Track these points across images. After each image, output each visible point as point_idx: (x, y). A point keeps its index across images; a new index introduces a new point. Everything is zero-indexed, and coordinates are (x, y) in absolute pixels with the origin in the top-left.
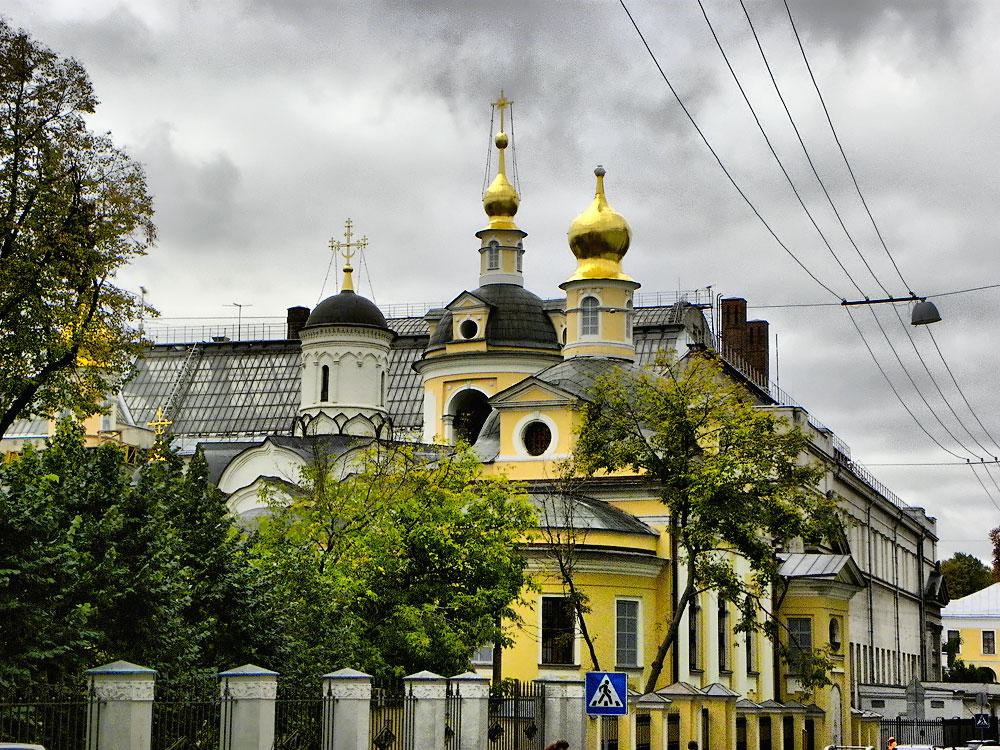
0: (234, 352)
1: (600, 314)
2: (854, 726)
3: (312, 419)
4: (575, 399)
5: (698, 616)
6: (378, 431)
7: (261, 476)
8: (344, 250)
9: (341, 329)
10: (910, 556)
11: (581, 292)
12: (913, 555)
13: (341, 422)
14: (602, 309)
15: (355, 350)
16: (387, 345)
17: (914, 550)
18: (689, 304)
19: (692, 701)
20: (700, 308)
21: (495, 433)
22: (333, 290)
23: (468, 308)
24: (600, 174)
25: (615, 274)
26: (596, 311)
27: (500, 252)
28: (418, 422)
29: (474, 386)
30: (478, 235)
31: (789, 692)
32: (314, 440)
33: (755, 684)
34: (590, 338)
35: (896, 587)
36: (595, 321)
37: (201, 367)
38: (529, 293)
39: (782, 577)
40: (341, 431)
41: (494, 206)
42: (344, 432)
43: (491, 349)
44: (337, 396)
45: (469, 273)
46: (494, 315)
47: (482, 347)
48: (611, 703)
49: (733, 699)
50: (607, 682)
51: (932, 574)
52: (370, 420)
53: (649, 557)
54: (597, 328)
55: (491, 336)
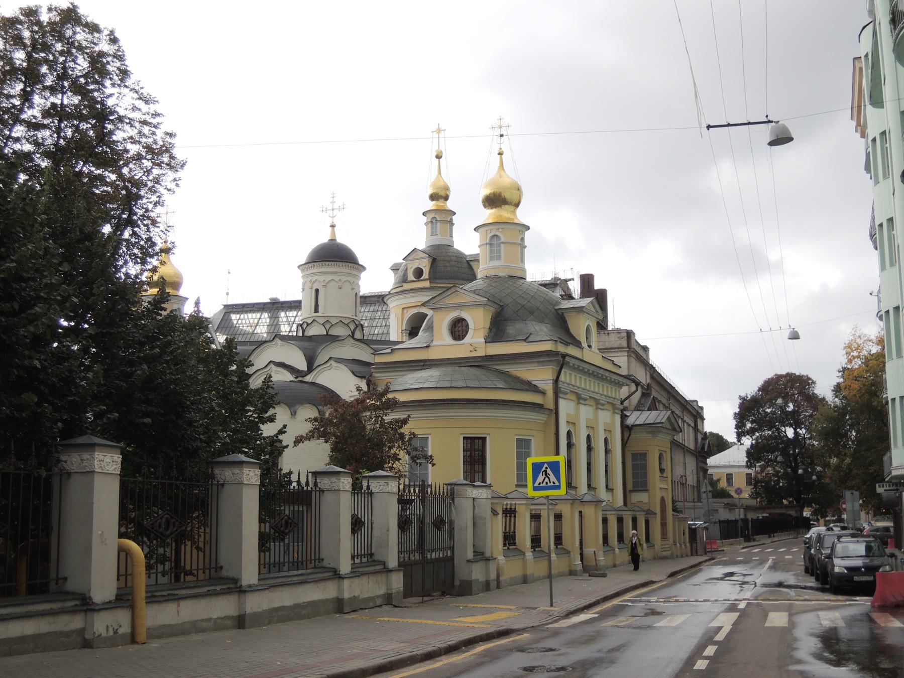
0: (282, 307)
1: (502, 245)
2: (674, 523)
3: (308, 325)
5: (573, 450)
6: (353, 333)
7: (271, 362)
8: (330, 213)
9: (327, 263)
10: (691, 428)
11: (489, 231)
12: (692, 427)
13: (328, 326)
14: (503, 243)
15: (337, 278)
17: (693, 425)
18: (560, 279)
19: (571, 504)
20: (566, 281)
22: (324, 239)
23: (417, 259)
24: (500, 154)
25: (513, 219)
26: (499, 245)
27: (438, 224)
30: (424, 214)
31: (633, 502)
32: (304, 338)
33: (611, 496)
35: (684, 445)
36: (499, 251)
37: (263, 317)
38: (457, 250)
39: (628, 426)
40: (327, 333)
42: (329, 333)
45: (420, 239)
46: (434, 261)
47: (427, 284)
48: (550, 482)
49: (600, 503)
50: (546, 468)
51: (702, 439)
52: (347, 325)
53: (538, 407)
54: (500, 256)
55: (433, 277)
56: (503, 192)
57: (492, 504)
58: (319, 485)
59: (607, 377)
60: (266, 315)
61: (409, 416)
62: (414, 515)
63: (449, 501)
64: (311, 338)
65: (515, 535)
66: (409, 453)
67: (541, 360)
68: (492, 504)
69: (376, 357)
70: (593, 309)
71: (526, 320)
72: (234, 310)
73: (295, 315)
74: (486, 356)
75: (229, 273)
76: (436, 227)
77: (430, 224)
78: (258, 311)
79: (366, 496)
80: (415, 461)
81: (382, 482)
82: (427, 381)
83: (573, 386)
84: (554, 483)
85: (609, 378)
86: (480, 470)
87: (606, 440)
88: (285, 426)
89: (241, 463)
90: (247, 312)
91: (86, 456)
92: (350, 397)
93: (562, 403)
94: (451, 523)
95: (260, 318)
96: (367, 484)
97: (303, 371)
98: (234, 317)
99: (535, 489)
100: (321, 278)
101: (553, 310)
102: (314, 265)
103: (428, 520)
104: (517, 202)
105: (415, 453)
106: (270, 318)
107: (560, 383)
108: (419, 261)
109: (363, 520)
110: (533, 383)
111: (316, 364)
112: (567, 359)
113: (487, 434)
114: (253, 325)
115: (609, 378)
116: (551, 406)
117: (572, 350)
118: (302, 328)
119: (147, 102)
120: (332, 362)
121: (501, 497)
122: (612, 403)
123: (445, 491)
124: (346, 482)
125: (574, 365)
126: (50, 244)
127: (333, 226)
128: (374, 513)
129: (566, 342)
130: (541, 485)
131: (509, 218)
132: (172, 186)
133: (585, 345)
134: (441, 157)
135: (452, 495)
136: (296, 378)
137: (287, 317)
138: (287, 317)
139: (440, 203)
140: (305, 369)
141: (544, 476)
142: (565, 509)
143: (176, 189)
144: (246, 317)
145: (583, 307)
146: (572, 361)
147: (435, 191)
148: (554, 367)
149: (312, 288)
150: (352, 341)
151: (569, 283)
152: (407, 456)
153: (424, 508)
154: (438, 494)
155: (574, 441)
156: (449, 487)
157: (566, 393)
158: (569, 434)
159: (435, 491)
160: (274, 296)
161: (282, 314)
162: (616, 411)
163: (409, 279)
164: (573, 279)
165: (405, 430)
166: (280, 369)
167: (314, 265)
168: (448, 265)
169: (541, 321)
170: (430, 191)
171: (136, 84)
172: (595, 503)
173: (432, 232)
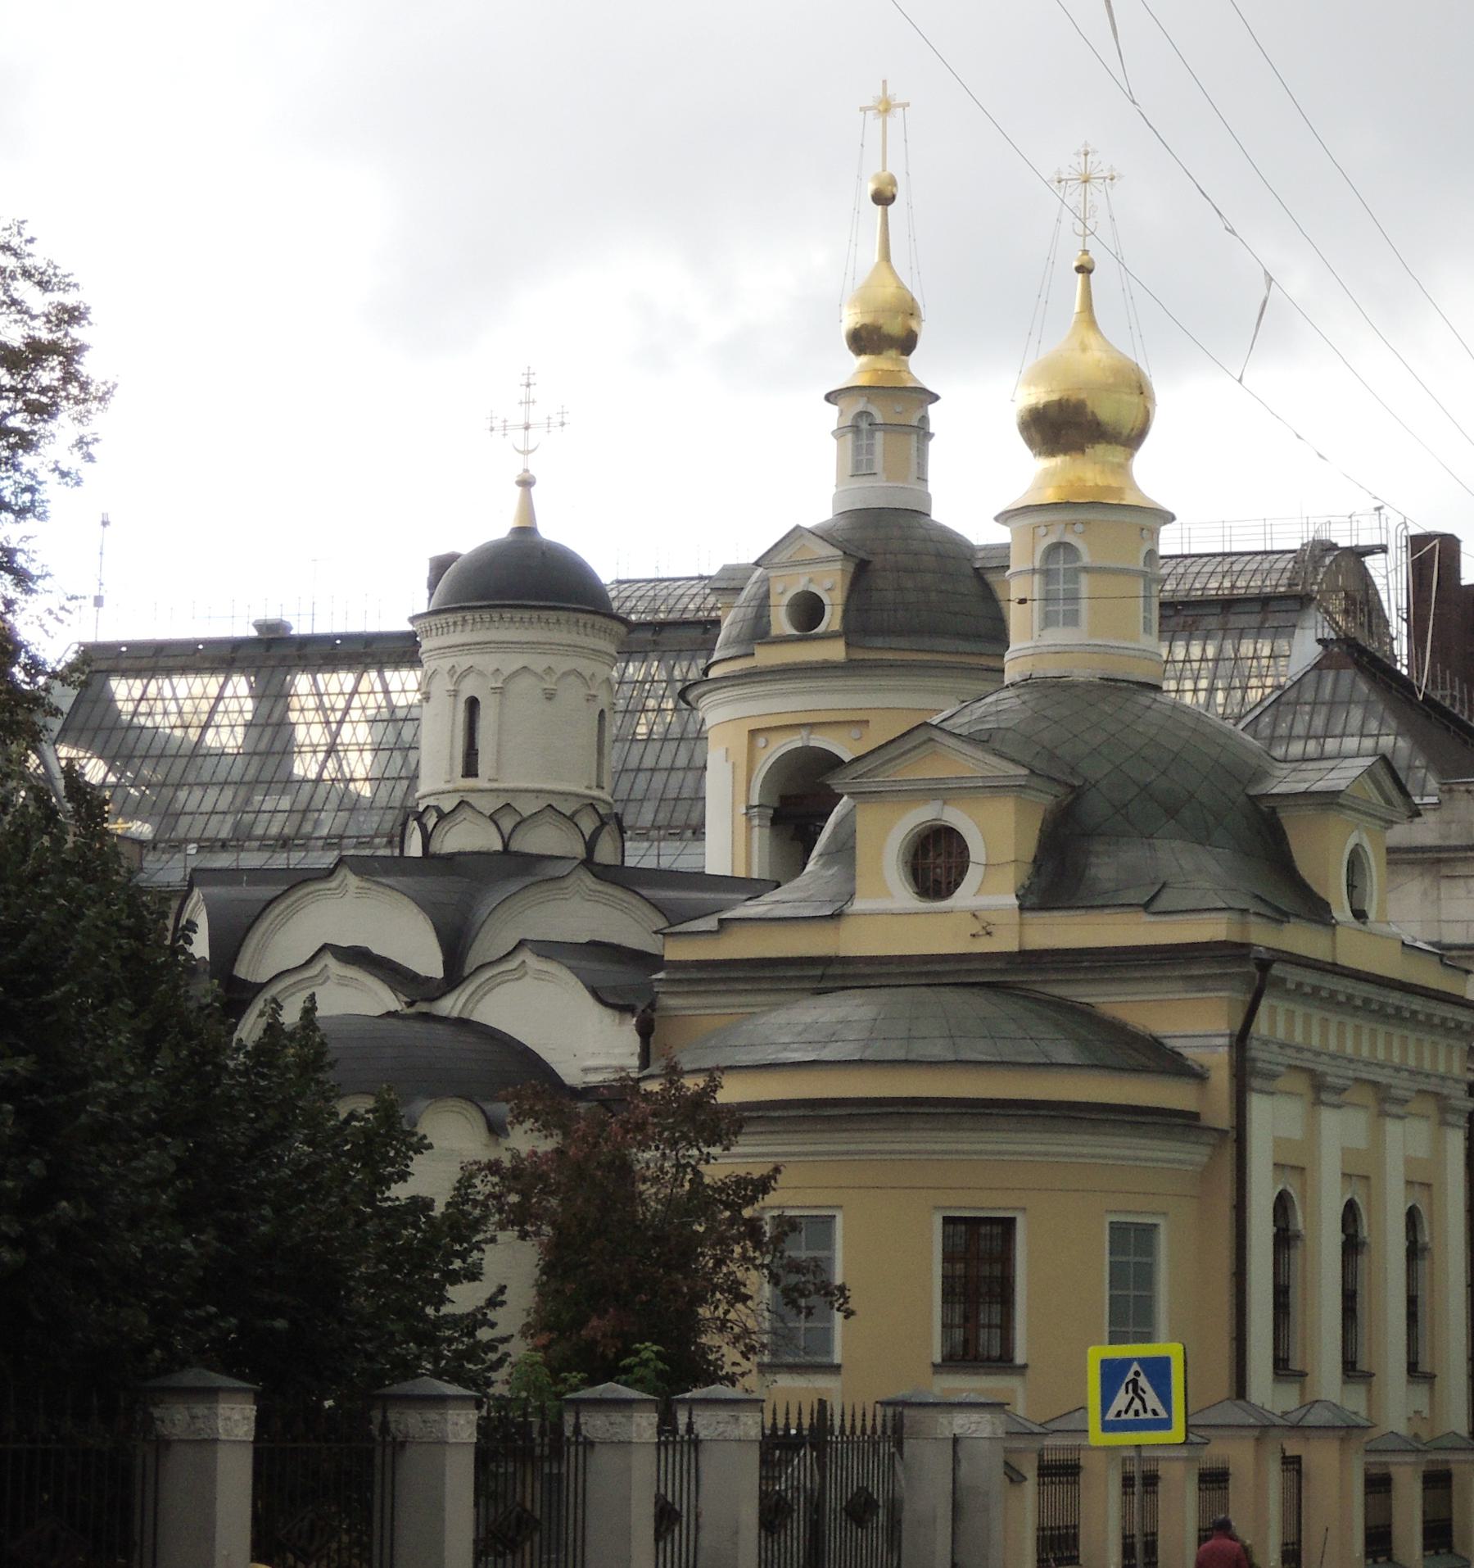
0: (299, 657)
1: (1084, 580)
3: (442, 816)
4: (1025, 772)
6: (590, 846)
7: (325, 948)
11: (1042, 530)
13: (507, 824)
14: (1086, 569)
15: (538, 663)
16: (612, 650)
18: (1334, 547)
19: (1257, 1439)
20: (1358, 554)
21: (844, 851)
22: (497, 527)
24: (1084, 269)
25: (1119, 491)
26: (1074, 574)
27: (879, 436)
28: (694, 821)
29: (820, 741)
30: (830, 397)
32: (433, 862)
33: (1426, 1400)
34: (1059, 636)
37: (228, 692)
40: (506, 845)
41: (864, 334)
42: (515, 846)
43: (859, 655)
44: (499, 766)
46: (861, 574)
47: (836, 651)
50: (1137, 1373)
52: (571, 818)
53: (1182, 1123)
55: (856, 629)
56: (1089, 403)
57: (1007, 1451)
58: (584, 1432)
59: (1414, 1013)
60: (240, 685)
61: (777, 1170)
62: (798, 1488)
63: (885, 1448)
64: (452, 863)
65: (1076, 1537)
66: (774, 1279)
67: (1196, 972)
68: (1007, 1451)
69: (670, 942)
70: (1376, 797)
71: (1151, 836)
72: (125, 664)
73: (348, 688)
74: (1022, 953)
75: (105, 524)
76: (870, 449)
77: (850, 436)
78: (213, 671)
79: (685, 1449)
80: (793, 1303)
81: (723, 1414)
82: (831, 1039)
83: (1299, 1049)
84: (1154, 1412)
85: (1421, 1017)
86: (997, 1320)
87: (1412, 1217)
88: (502, 1290)
89: (441, 1400)
90: (169, 672)
91: (200, 1410)
92: (586, 1070)
93: (1259, 1107)
94: (895, 1509)
95: (219, 698)
96: (687, 1420)
97: (429, 979)
98: (123, 690)
99: (1107, 1427)
100: (486, 662)
101: (1242, 798)
102: (464, 620)
103: (834, 1500)
104: (1138, 424)
105: (793, 1279)
106: (257, 695)
107: (1255, 1043)
108: (808, 569)
109: (677, 1507)
110: (1169, 1043)
111: (473, 960)
112: (1277, 970)
113: (1015, 1209)
114: (195, 722)
115: (1421, 1017)
116: (1220, 1114)
117: (1300, 939)
118: (423, 827)
119: (44, 285)
120: (526, 956)
121: (1032, 1433)
122: (1436, 1095)
123: (879, 1420)
124: (644, 1423)
125: (1299, 985)
126: (127, 1005)
127: (526, 483)
128: (702, 1490)
129: (1277, 909)
130: (1124, 1416)
131: (1108, 489)
132: (72, 461)
133: (1342, 911)
134: (893, 198)
135: (897, 1433)
136: (410, 1004)
137: (319, 695)
138: (319, 695)
139: (884, 362)
140: (439, 973)
141: (1131, 1394)
142: (1237, 1454)
143: (86, 470)
144: (168, 693)
145: (1337, 793)
146: (1294, 975)
147: (867, 320)
148: (1235, 995)
149: (455, 694)
150: (588, 881)
151: (1370, 561)
152: (767, 1289)
153: (823, 1478)
154: (858, 1432)
155: (1300, 1226)
156: (890, 1411)
157: (1273, 1076)
158: (1282, 1205)
159: (853, 1427)
160: (272, 615)
161: (302, 682)
162: (1451, 1118)
163: (775, 631)
164: (1384, 549)
165: (767, 1209)
166: (352, 972)
167: (464, 620)
168: (910, 584)
169: (1203, 838)
170: (851, 319)
171: (15, 230)
172: (1342, 1433)
173: (857, 464)
